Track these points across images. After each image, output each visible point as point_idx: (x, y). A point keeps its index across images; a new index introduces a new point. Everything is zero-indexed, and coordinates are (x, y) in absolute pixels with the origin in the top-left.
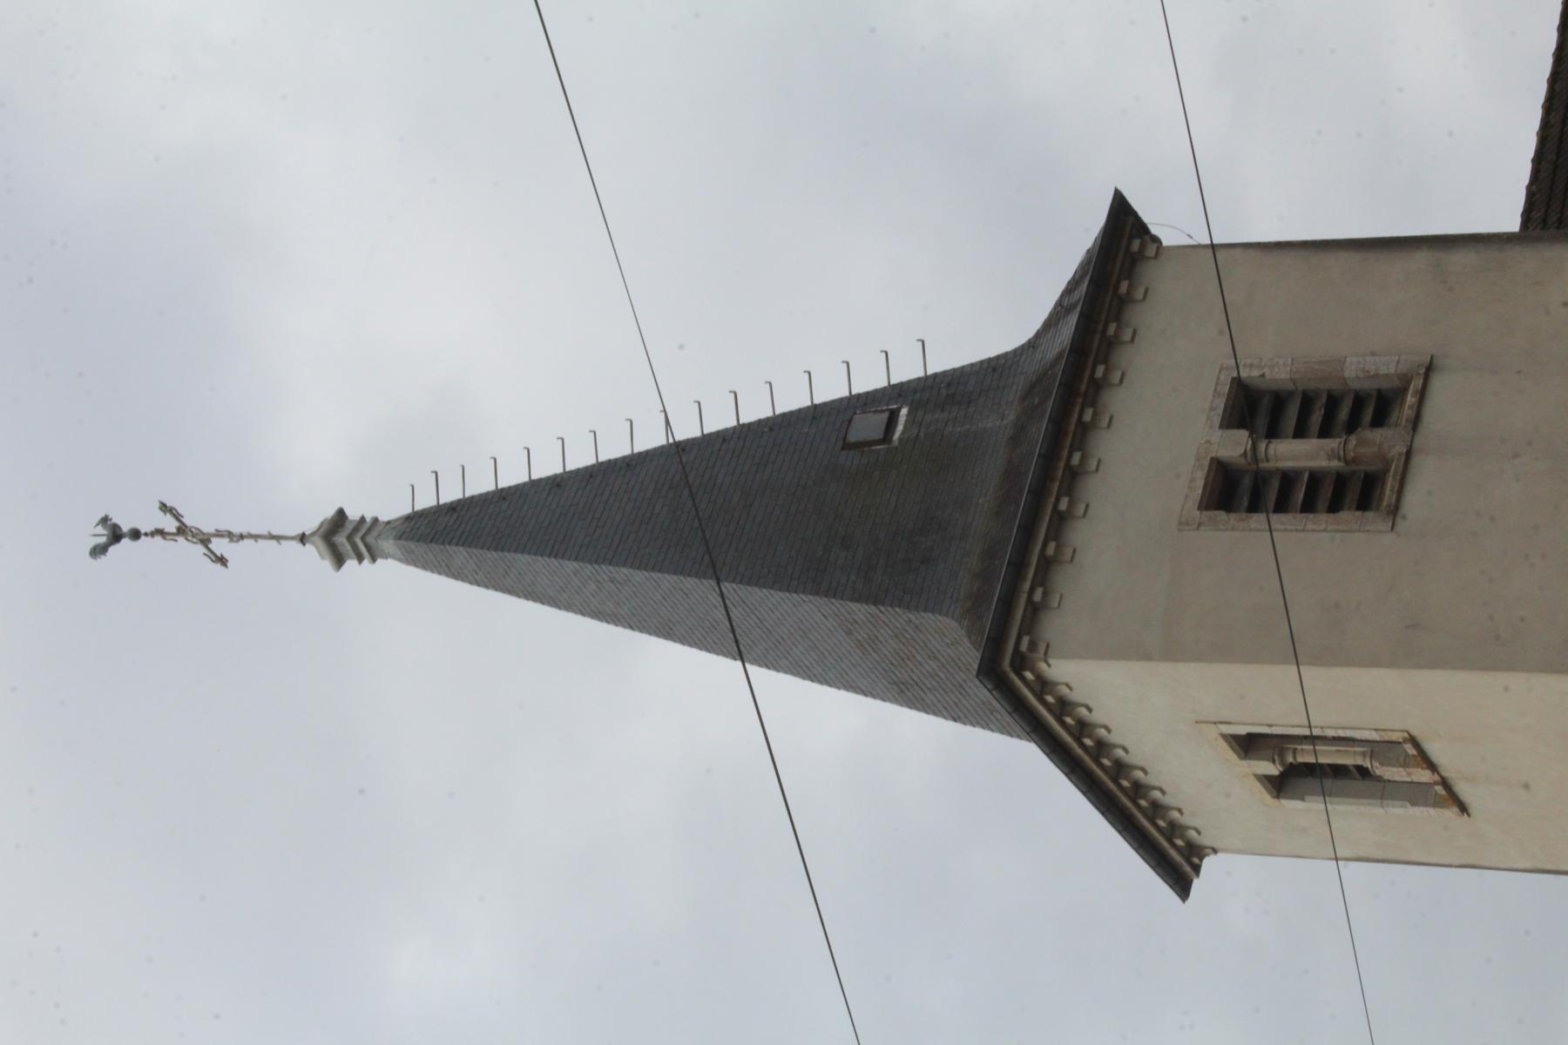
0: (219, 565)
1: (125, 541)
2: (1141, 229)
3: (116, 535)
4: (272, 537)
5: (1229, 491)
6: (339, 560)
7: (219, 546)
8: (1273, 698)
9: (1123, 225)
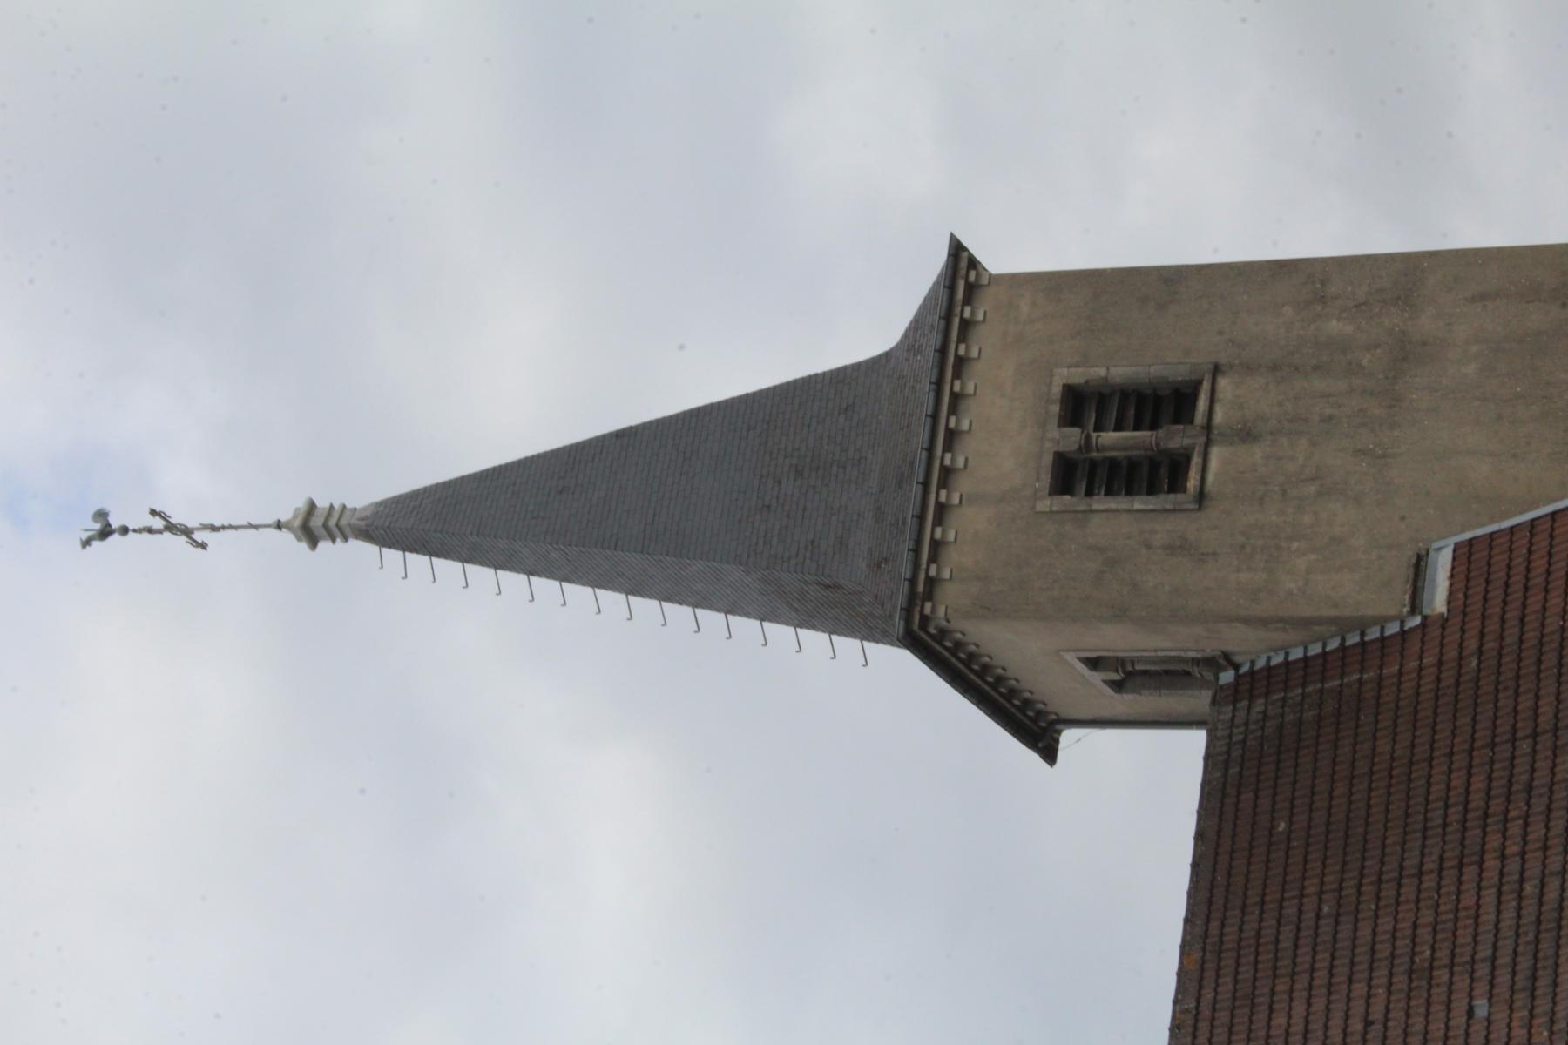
0: (199, 550)
1: (116, 537)
2: (973, 263)
3: (105, 533)
4: (256, 527)
5: (1068, 475)
6: (313, 542)
7: (158, 523)
8: (1120, 639)
9: (960, 262)
